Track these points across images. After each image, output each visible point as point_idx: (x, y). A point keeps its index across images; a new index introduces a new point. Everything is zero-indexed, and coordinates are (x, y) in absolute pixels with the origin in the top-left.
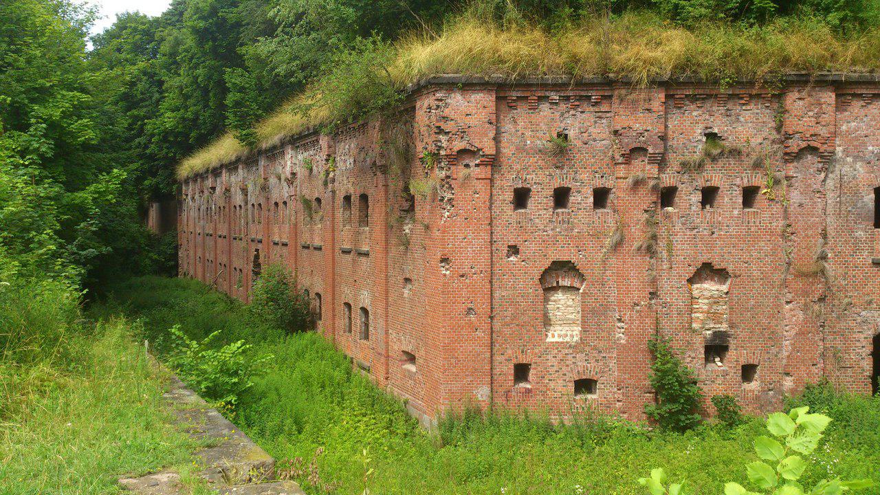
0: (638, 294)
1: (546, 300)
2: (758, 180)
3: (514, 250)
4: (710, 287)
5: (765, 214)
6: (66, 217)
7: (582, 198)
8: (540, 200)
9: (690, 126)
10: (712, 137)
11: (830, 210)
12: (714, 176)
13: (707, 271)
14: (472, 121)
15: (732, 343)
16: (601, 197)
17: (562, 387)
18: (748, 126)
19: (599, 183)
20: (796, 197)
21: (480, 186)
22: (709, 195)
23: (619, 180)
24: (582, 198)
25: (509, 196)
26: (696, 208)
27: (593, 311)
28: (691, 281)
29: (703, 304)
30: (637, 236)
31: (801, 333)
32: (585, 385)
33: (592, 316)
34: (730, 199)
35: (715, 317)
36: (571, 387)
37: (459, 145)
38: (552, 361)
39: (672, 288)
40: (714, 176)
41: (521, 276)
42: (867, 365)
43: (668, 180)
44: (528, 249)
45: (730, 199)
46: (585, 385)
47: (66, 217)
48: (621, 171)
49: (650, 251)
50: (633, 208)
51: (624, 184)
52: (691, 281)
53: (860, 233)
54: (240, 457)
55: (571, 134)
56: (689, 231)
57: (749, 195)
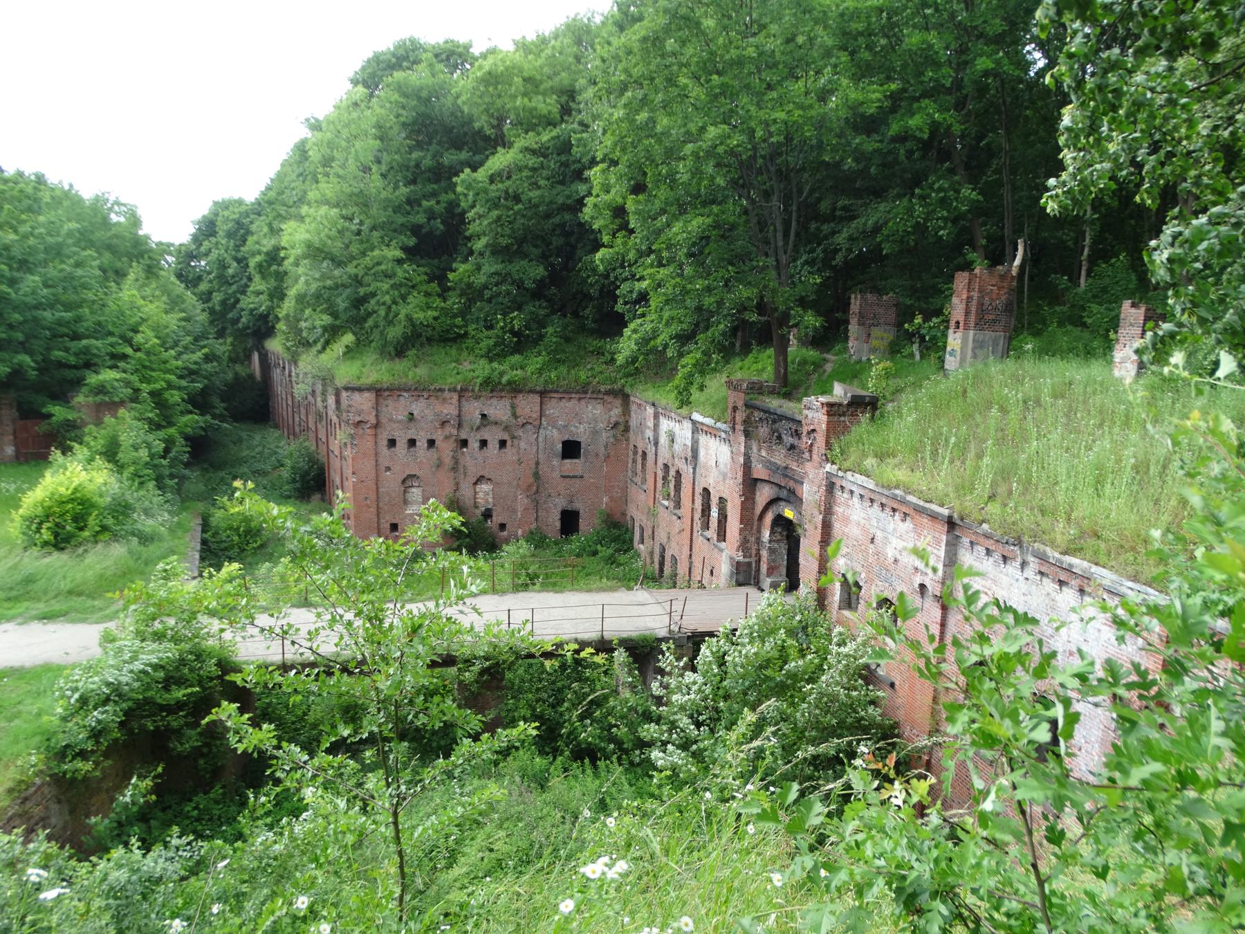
1: (405, 492)
3: (388, 469)
4: (485, 487)
5: (509, 451)
7: (422, 444)
8: (402, 444)
10: (484, 416)
12: (485, 434)
13: (480, 479)
14: (365, 408)
15: (494, 514)
16: (431, 443)
20: (523, 445)
22: (484, 443)
23: (438, 436)
24: (422, 444)
25: (385, 443)
26: (477, 449)
29: (481, 495)
30: (448, 461)
34: (493, 445)
40: (485, 434)
41: (391, 482)
42: (558, 524)
43: (463, 436)
44: (396, 468)
45: (493, 445)
50: (446, 449)
51: (441, 438)
52: (475, 484)
55: (415, 413)
57: (503, 444)
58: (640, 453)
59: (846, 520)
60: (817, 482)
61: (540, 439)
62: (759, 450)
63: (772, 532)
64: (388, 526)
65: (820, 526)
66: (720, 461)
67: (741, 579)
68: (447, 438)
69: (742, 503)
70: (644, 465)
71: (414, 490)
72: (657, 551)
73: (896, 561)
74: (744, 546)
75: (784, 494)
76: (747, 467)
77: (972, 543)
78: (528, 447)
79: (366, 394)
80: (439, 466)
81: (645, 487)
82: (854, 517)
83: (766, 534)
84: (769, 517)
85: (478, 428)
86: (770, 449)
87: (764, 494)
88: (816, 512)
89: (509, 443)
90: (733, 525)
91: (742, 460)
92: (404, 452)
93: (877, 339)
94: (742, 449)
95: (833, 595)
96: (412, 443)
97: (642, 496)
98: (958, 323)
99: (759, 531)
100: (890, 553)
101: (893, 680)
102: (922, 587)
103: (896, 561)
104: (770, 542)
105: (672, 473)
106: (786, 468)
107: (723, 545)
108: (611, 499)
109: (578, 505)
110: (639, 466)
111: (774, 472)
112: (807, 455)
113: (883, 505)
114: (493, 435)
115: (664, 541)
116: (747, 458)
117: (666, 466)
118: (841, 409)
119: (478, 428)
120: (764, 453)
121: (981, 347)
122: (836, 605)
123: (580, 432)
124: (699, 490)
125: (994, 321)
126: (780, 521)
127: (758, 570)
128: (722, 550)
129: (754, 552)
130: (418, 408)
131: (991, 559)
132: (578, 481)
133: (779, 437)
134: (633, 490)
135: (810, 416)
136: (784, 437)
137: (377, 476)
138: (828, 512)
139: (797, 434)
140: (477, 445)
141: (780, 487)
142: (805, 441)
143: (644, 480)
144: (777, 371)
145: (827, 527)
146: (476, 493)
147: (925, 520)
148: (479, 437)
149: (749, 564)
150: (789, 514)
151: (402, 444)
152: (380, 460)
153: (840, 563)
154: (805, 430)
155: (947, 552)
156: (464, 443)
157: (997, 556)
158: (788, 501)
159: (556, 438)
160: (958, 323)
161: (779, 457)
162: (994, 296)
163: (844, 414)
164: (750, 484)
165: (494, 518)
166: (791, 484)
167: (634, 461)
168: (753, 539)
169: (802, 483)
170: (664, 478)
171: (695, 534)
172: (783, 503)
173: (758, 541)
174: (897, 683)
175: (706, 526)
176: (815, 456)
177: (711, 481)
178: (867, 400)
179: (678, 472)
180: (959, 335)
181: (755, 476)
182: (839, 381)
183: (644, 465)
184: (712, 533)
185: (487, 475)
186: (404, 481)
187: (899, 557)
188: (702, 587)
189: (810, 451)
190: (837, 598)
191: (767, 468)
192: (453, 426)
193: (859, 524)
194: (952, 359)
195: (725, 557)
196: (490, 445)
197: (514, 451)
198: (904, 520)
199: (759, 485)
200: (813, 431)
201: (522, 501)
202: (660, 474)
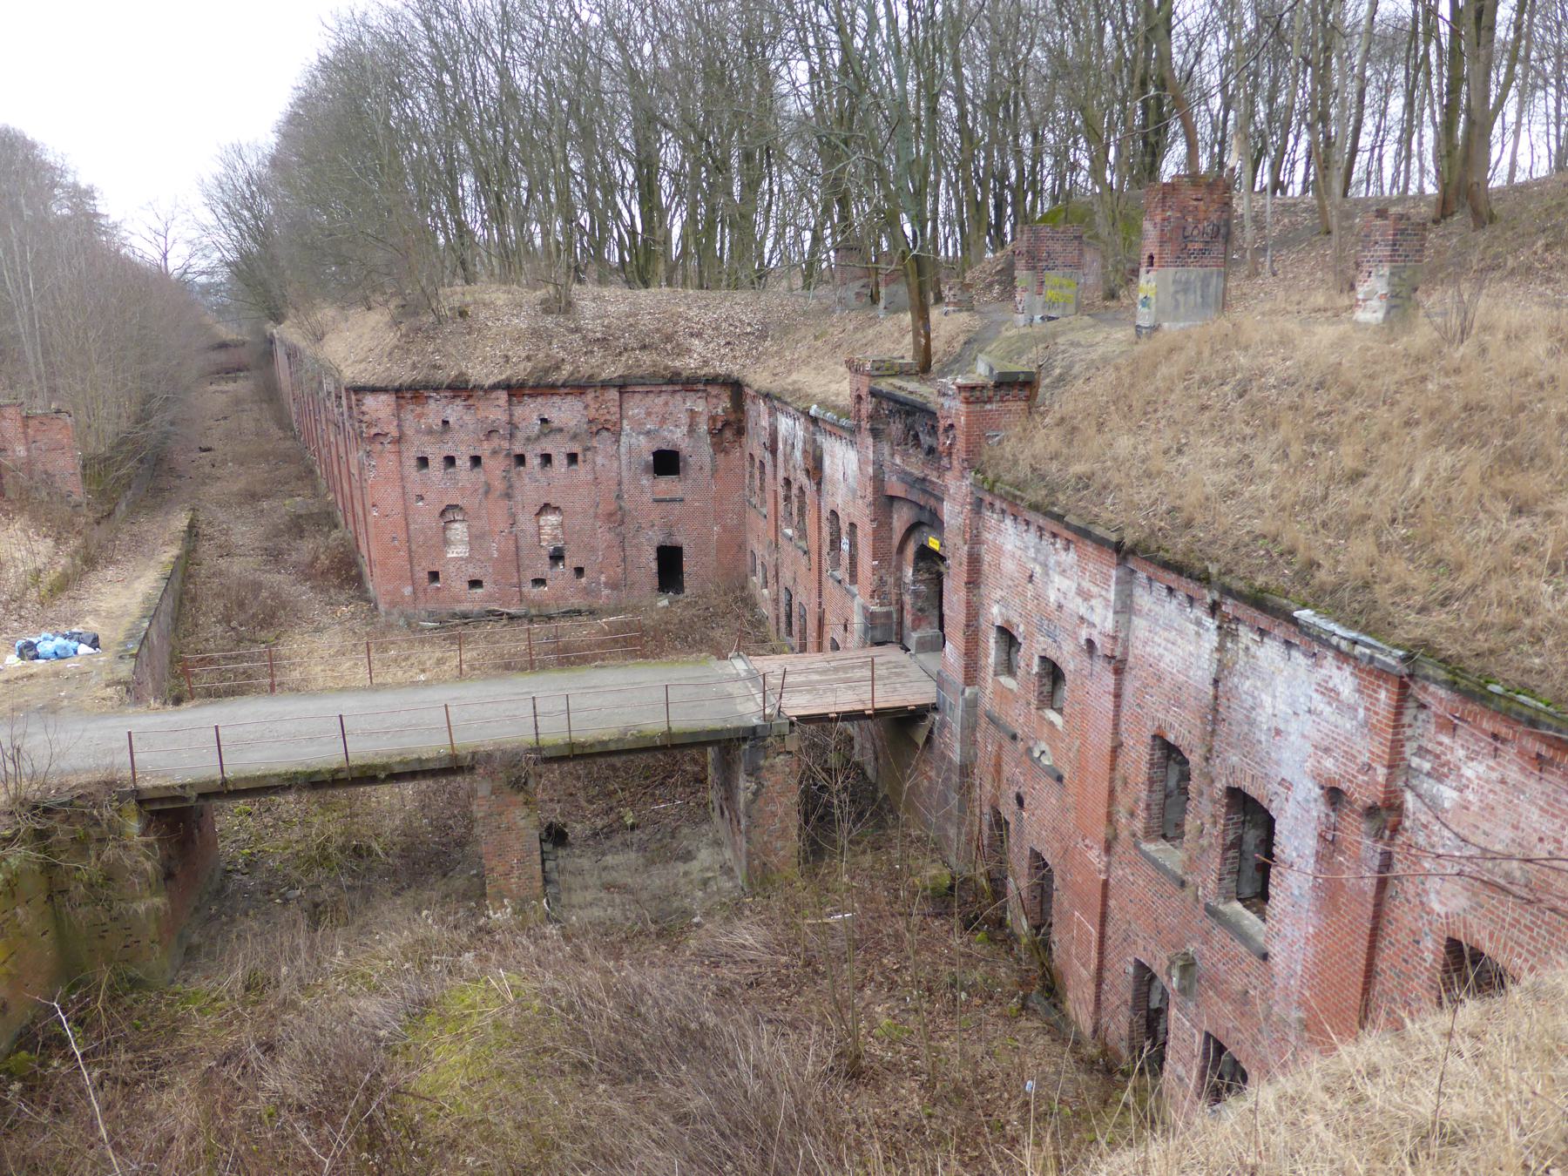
0: (503, 525)
1: (445, 529)
2: (576, 448)
3: (421, 498)
4: (552, 519)
5: (582, 471)
6: (676, 232)
7: (463, 462)
8: (436, 463)
9: (530, 412)
10: (544, 421)
11: (624, 467)
12: (548, 446)
13: (546, 508)
14: (382, 415)
15: (567, 555)
16: (476, 461)
17: (460, 586)
18: (566, 412)
19: (473, 453)
20: (600, 460)
21: (392, 457)
22: (547, 459)
23: (484, 450)
24: (463, 462)
25: (414, 462)
26: (537, 468)
27: (477, 537)
28: (539, 514)
29: (547, 530)
30: (499, 485)
31: (608, 547)
32: (475, 584)
33: (475, 539)
34: (559, 461)
35: (555, 538)
36: (467, 586)
37: (374, 431)
38: (452, 569)
39: (526, 522)
40: (548, 446)
41: (425, 516)
42: (654, 566)
43: (518, 450)
44: (430, 496)
45: (559, 461)
46: (475, 584)
47: (676, 232)
48: (486, 445)
49: (508, 496)
50: (495, 467)
51: (487, 453)
52: (539, 514)
53: (644, 482)
54: (326, 99)
55: (451, 420)
56: (532, 484)
57: (572, 458)
58: (757, 463)
59: (999, 550)
60: (959, 498)
61: (623, 450)
62: (892, 455)
63: (916, 571)
64: (425, 575)
65: (965, 560)
66: (849, 472)
67: (879, 636)
68: (495, 452)
69: (875, 531)
70: (762, 480)
71: (457, 525)
72: (783, 597)
73: (1060, 607)
74: (878, 592)
75: (925, 517)
76: (878, 480)
77: (1150, 579)
78: (606, 463)
79: (383, 397)
80: (488, 491)
81: (764, 511)
82: (1009, 547)
83: (909, 573)
84: (911, 549)
85: (538, 438)
86: (905, 454)
87: (901, 519)
88: (960, 542)
89: (580, 458)
90: (866, 562)
91: (871, 470)
92: (440, 474)
93: (1053, 288)
94: (871, 456)
95: (987, 656)
96: (450, 461)
97: (762, 524)
98: (1151, 257)
99: (899, 568)
100: (1053, 596)
101: (1062, 771)
102: (1090, 642)
103: (1060, 607)
104: (914, 583)
105: (795, 491)
106: (924, 480)
107: (855, 589)
108: (724, 527)
109: (680, 539)
110: (757, 483)
111: (912, 487)
112: (945, 462)
113: (1040, 529)
114: (558, 448)
115: (790, 584)
116: (879, 466)
117: (788, 482)
118: (986, 393)
119: (538, 438)
120: (898, 460)
121: (1186, 291)
122: (991, 671)
123: (676, 436)
124: (825, 514)
125: (1202, 252)
126: (925, 554)
127: (901, 623)
128: (854, 596)
129: (894, 598)
130: (454, 412)
131: (1175, 602)
132: (677, 505)
133: (916, 436)
134: (751, 515)
135: (946, 405)
136: (921, 436)
137: (406, 508)
138: (975, 540)
139: (933, 430)
140: (537, 461)
141: (921, 508)
142: (944, 441)
143: (763, 502)
144: (916, 342)
145: (974, 561)
146: (540, 527)
147: (1090, 549)
148: (539, 451)
149: (888, 615)
150: (934, 544)
151: (436, 463)
152: (408, 485)
153: (995, 613)
154: (943, 424)
155: (1117, 593)
156: (521, 460)
157: (1181, 596)
158: (931, 526)
159: (645, 448)
160: (1151, 257)
161: (915, 465)
162: (1201, 216)
163: (990, 400)
164: (885, 503)
165: (567, 561)
166: (932, 502)
167: (752, 476)
168: (891, 580)
169: (942, 500)
170: (787, 498)
171: (824, 575)
172: (926, 529)
173: (899, 582)
174: (1066, 776)
175: (836, 564)
176: (955, 463)
177: (839, 501)
178: (1022, 378)
179: (801, 488)
180: (1152, 275)
181: (890, 493)
182: (146, 287)
183: (762, 480)
184: (842, 573)
185: (554, 503)
186: (443, 513)
187: (1063, 601)
188: (835, 647)
189: (950, 454)
190: (992, 660)
191: (903, 481)
192: (503, 437)
193: (1013, 556)
194: (1145, 310)
195: (857, 605)
196: (555, 461)
197: (589, 467)
198: (1067, 549)
199: (896, 505)
200: (952, 426)
201: (604, 536)
202: (781, 492)
